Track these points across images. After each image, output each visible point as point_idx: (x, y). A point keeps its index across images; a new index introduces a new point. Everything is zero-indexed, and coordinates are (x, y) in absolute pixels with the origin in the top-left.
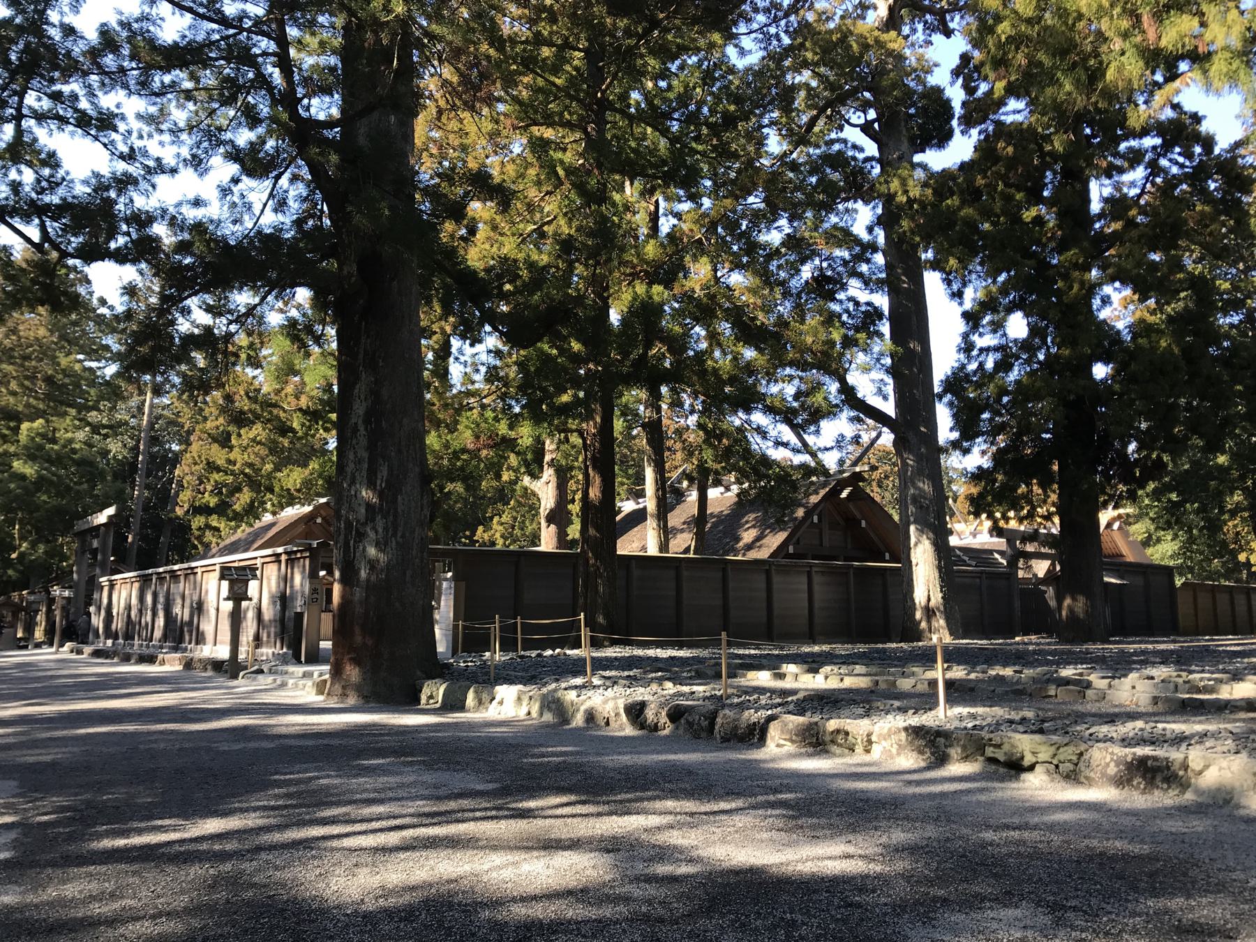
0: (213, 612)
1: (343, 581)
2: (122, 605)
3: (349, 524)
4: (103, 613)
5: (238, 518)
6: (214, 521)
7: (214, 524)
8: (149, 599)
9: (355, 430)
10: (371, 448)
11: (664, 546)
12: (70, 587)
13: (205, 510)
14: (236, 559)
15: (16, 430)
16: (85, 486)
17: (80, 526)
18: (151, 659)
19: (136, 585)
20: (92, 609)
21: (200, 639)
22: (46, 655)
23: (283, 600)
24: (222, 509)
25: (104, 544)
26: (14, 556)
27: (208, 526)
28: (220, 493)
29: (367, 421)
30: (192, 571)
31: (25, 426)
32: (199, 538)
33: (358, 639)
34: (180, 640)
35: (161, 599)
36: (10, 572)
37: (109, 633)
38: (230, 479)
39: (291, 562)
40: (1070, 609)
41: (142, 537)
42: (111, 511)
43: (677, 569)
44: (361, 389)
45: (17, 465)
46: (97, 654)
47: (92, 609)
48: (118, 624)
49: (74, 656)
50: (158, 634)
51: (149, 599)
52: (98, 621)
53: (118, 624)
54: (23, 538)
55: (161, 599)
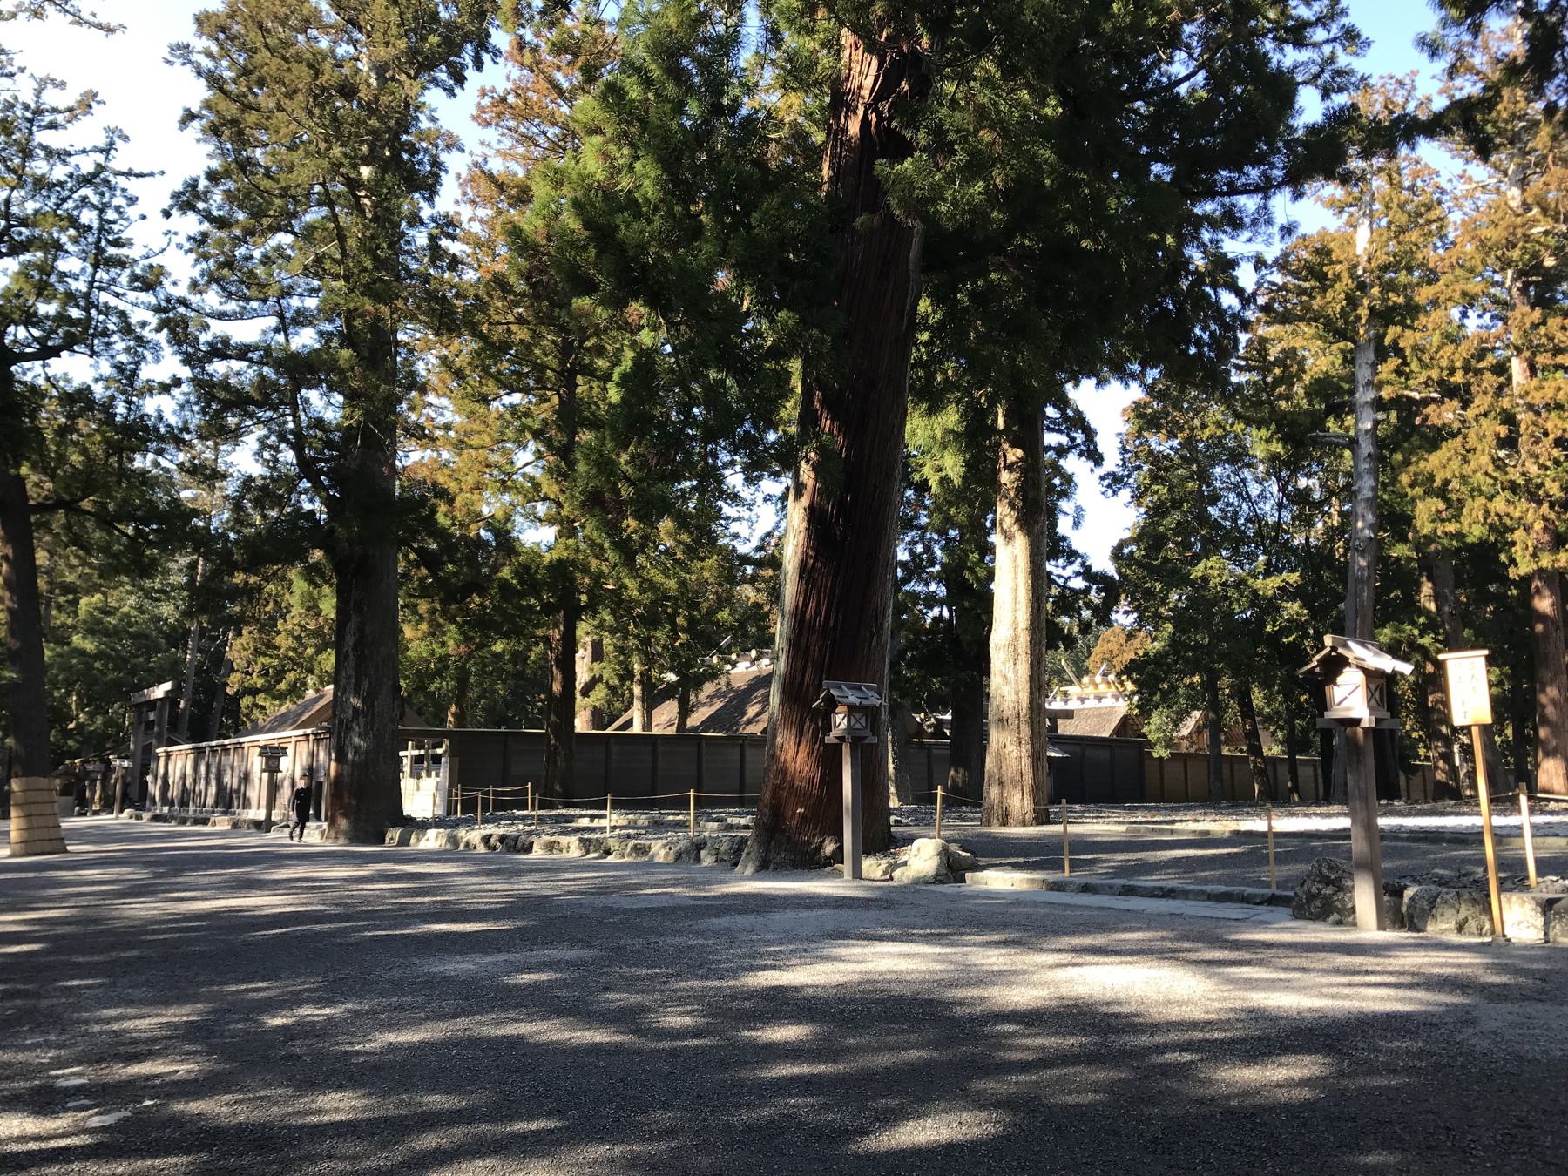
0: (257, 781)
1: (337, 760)
2: (178, 774)
3: (341, 721)
4: (159, 782)
5: (282, 697)
6: (261, 699)
7: (261, 703)
8: (203, 769)
9: (347, 656)
10: (357, 667)
11: (647, 725)
12: (126, 757)
13: (253, 692)
14: (273, 738)
15: (75, 602)
16: (141, 659)
17: (136, 698)
18: (205, 822)
19: (191, 757)
20: (149, 778)
21: (246, 804)
22: (106, 819)
23: (310, 772)
24: (267, 690)
25: (160, 717)
26: (71, 726)
27: (255, 705)
28: (267, 674)
29: (355, 649)
30: (240, 746)
31: (84, 601)
32: (247, 715)
33: (346, 800)
34: (230, 805)
35: (214, 770)
36: (70, 743)
37: (165, 800)
38: (276, 662)
39: (317, 741)
40: (953, 780)
41: (194, 702)
42: (167, 686)
43: (654, 745)
44: (352, 626)
45: (76, 640)
46: (156, 818)
47: (149, 778)
48: (174, 792)
49: (133, 821)
50: (210, 801)
51: (203, 769)
52: (155, 790)
53: (174, 792)
54: (81, 707)
55: (214, 770)
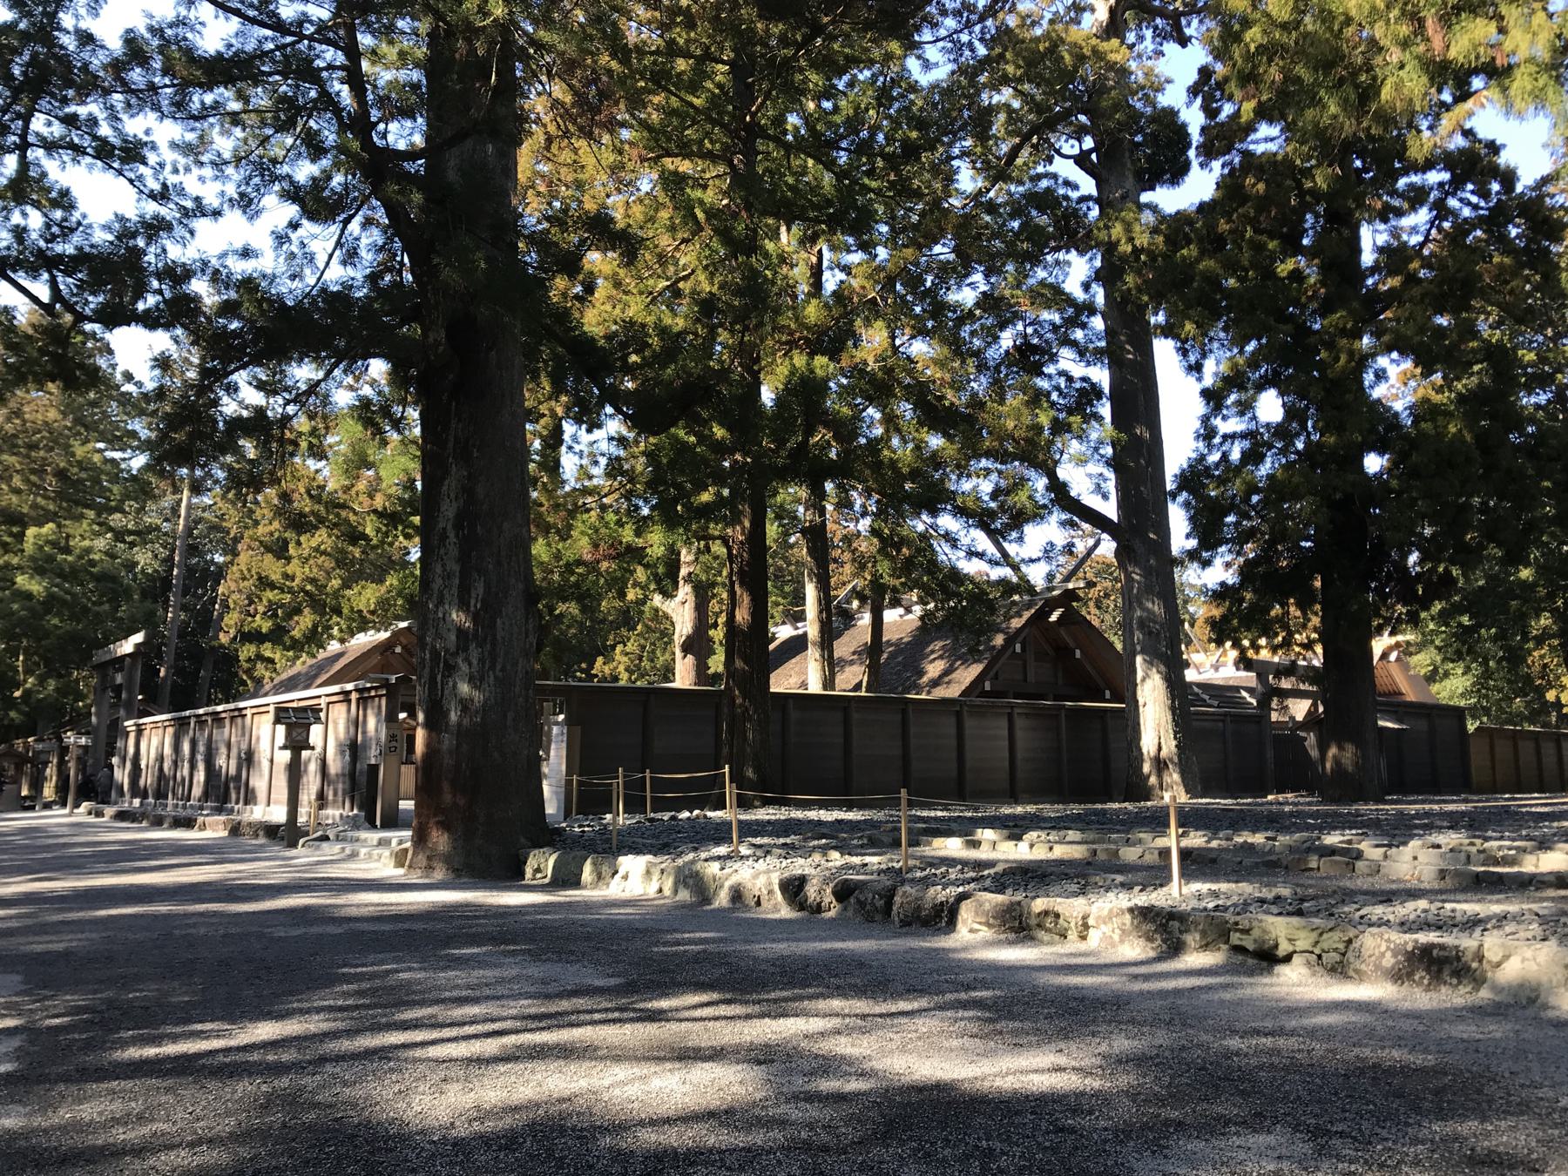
0: (265, 765)
1: (428, 725)
2: (153, 755)
3: (435, 654)
4: (128, 765)
5: (297, 646)
6: (267, 650)
7: (268, 654)
8: (186, 747)
9: (444, 537)
10: (463, 559)
11: (829, 682)
12: (87, 733)
13: (256, 637)
14: (295, 697)
15: (20, 537)
16: (106, 607)
17: (100, 656)
18: (188, 823)
19: (170, 730)
20: (115, 760)
21: (250, 798)
22: (58, 817)
23: (354, 749)
24: (278, 635)
25: (130, 679)
26: (17, 694)
27: (259, 657)
28: (275, 615)
29: (458, 526)
30: (240, 713)
31: (31, 532)
32: (249, 672)
33: (447, 798)
34: (225, 798)
35: (201, 748)
36: (13, 714)
37: (136, 791)
38: (287, 598)
39: (363, 701)
40: (1336, 760)
41: (177, 670)
42: (138, 638)
43: (846, 710)
44: (450, 485)
45: (21, 580)
46: (121, 816)
47: (115, 760)
48: (147, 779)
49: (92, 819)
50: (197, 791)
51: (186, 747)
52: (122, 776)
53: (147, 779)
54: (28, 672)
55: (201, 748)
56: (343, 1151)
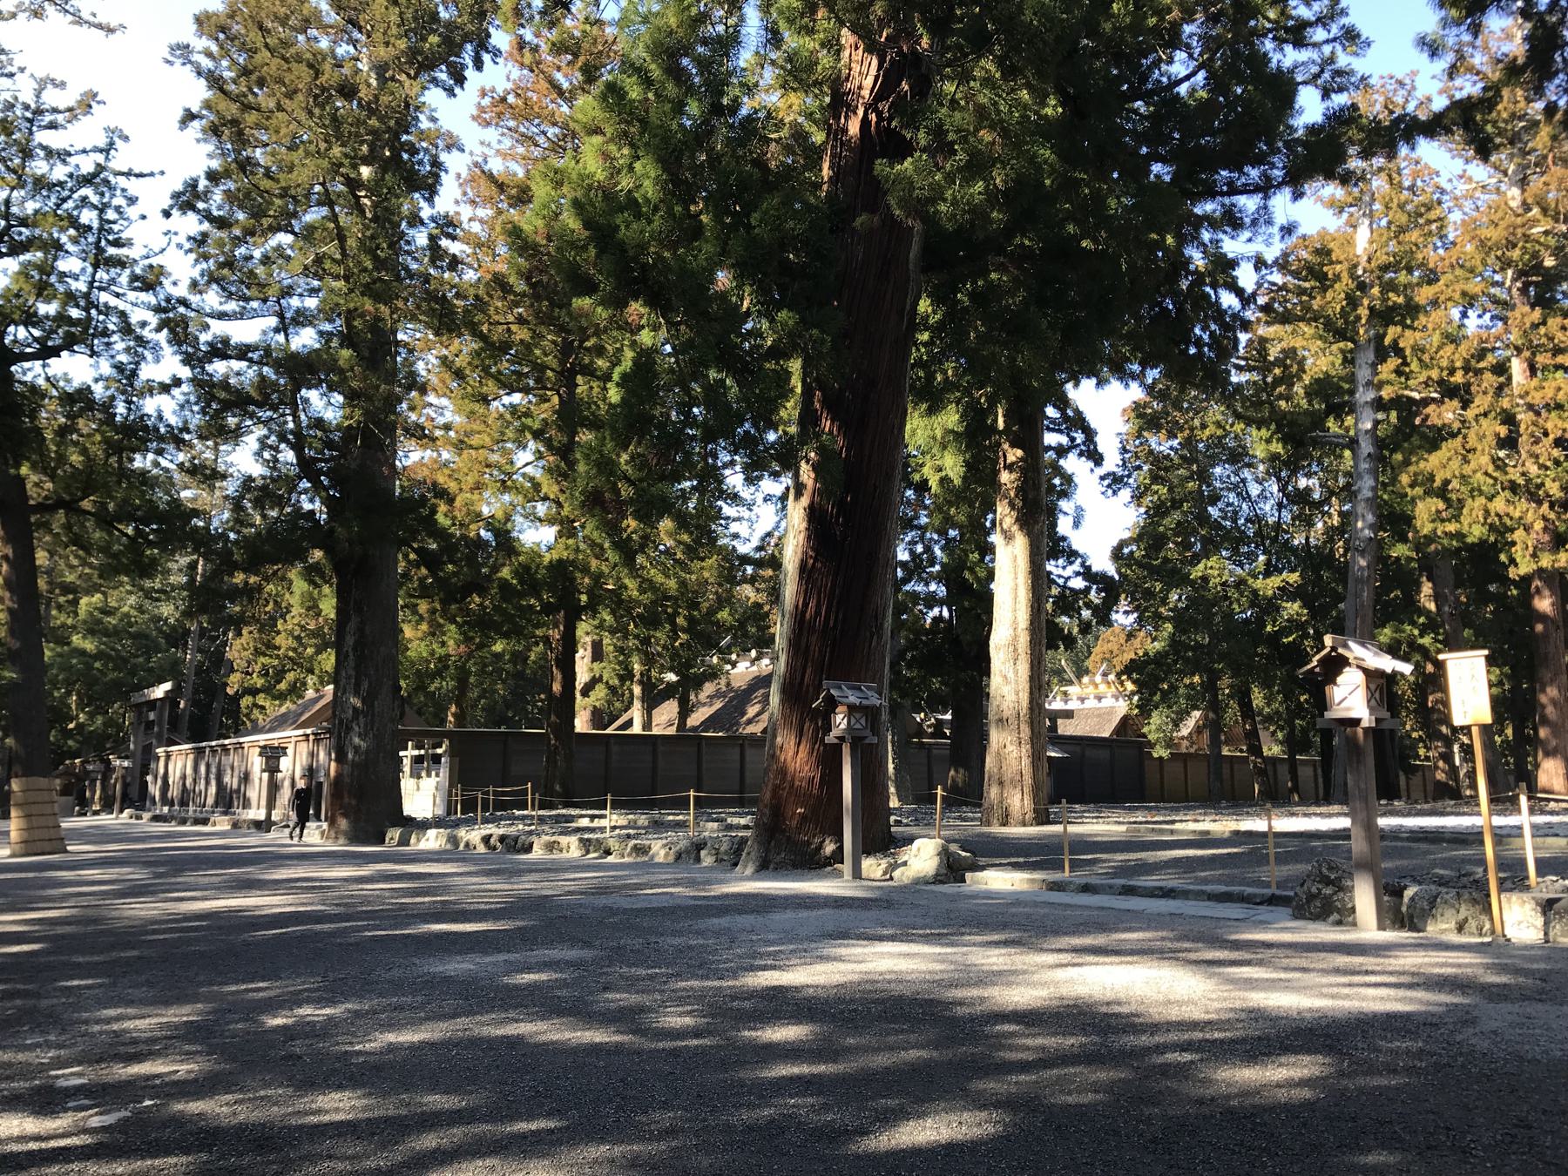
0: (257, 781)
1: (337, 760)
2: (178, 774)
3: (341, 721)
4: (159, 782)
5: (282, 697)
6: (261, 699)
7: (261, 703)
8: (203, 769)
9: (347, 656)
10: (357, 667)
11: (647, 725)
12: (126, 757)
13: (253, 692)
14: (273, 738)
15: (75, 602)
16: (141, 659)
17: (136, 698)
18: (205, 822)
19: (191, 757)
20: (149, 778)
21: (246, 804)
22: (106, 819)
23: (310, 772)
24: (267, 690)
25: (160, 717)
26: (71, 726)
27: (255, 705)
28: (267, 674)
29: (355, 649)
30: (240, 746)
31: (84, 601)
32: (247, 715)
33: (346, 800)
34: (230, 805)
35: (214, 770)
36: (70, 743)
37: (165, 800)
38: (276, 662)
39: (317, 741)
40: (953, 780)
41: (194, 702)
42: (167, 686)
43: (654, 745)
44: (352, 626)
45: (76, 640)
46: (156, 818)
47: (149, 778)
48: (174, 792)
49: (133, 821)
50: (210, 801)
51: (203, 769)
52: (155, 790)
53: (174, 792)
54: (81, 707)
55: (214, 770)
56: (101, 318)
